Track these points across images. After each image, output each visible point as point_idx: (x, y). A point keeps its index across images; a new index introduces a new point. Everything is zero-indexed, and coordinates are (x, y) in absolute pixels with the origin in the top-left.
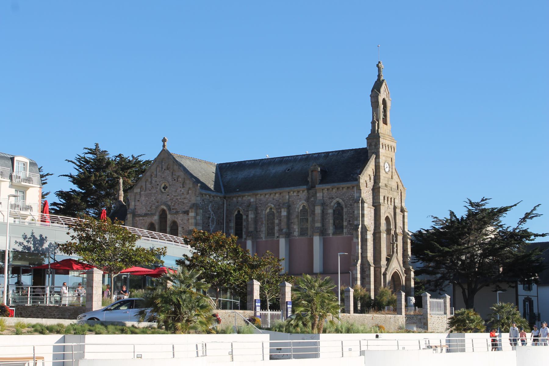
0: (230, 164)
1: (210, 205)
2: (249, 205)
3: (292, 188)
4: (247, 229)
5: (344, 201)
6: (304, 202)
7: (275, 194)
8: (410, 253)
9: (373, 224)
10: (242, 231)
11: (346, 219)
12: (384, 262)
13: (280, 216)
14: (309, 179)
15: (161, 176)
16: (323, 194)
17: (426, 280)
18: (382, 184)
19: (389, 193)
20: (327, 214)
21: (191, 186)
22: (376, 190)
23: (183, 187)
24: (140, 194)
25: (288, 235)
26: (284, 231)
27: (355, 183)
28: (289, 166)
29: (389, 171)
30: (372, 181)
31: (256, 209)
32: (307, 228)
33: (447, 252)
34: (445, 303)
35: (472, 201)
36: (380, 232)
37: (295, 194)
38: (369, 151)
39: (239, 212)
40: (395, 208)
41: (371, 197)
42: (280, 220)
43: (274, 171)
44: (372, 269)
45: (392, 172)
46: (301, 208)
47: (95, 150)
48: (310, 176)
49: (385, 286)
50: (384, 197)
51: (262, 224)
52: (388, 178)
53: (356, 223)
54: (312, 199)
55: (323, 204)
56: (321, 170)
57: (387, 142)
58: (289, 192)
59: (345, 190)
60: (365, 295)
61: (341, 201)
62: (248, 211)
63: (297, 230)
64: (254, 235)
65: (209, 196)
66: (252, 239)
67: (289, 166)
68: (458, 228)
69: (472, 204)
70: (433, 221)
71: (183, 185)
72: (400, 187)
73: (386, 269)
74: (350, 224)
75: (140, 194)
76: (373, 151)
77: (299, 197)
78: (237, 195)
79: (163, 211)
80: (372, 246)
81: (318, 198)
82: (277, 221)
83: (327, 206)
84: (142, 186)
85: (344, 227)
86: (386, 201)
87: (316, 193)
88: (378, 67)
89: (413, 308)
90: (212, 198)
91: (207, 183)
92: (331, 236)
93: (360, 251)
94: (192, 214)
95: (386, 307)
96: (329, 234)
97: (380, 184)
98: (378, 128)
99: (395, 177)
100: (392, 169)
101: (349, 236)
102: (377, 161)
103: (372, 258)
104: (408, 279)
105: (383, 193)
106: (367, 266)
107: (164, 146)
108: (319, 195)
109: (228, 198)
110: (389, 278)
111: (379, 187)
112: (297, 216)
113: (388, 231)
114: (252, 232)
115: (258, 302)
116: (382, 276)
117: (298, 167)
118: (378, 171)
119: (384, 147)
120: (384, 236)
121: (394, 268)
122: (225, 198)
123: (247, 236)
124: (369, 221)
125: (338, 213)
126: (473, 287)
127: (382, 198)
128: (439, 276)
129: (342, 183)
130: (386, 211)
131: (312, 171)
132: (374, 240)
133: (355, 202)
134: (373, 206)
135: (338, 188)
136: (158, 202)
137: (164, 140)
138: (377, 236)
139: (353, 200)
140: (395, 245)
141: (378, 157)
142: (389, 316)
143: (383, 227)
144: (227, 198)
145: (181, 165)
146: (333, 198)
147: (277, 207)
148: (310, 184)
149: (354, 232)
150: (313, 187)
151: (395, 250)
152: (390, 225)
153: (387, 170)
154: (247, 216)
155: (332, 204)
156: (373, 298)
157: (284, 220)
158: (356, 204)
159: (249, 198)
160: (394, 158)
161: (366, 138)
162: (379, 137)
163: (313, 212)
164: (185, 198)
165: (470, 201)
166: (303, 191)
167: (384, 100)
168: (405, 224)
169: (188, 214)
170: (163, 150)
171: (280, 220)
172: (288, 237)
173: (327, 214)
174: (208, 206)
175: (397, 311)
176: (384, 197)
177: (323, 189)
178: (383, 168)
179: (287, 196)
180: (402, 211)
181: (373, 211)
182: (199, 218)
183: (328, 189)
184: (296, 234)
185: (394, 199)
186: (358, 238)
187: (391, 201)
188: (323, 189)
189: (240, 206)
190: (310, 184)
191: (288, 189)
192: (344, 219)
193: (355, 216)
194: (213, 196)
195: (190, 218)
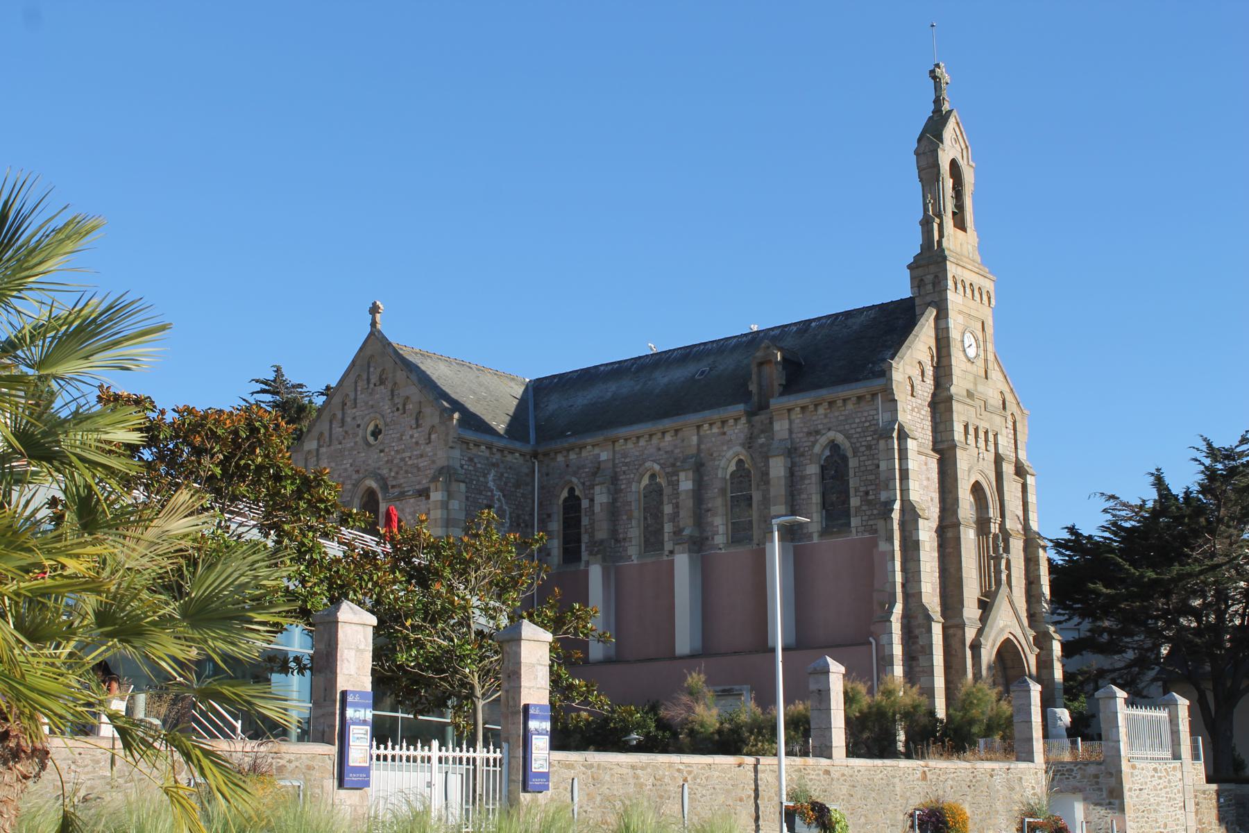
0: (561, 376)
1: (493, 473)
2: (597, 469)
3: (707, 414)
4: (592, 536)
5: (848, 437)
6: (738, 449)
7: (663, 433)
8: (1046, 590)
9: (937, 500)
10: (579, 541)
11: (857, 490)
12: (971, 611)
13: (676, 494)
14: (753, 387)
15: (367, 403)
16: (791, 422)
17: (1095, 667)
18: (958, 386)
19: (979, 416)
20: (803, 478)
21: (436, 420)
22: (941, 405)
23: (418, 426)
24: (318, 455)
25: (698, 544)
26: (687, 532)
27: (877, 383)
28: (704, 366)
29: (978, 355)
30: (930, 381)
31: (615, 480)
32: (751, 522)
33: (1154, 582)
34: (1174, 721)
35: (1216, 445)
36: (957, 525)
37: (715, 430)
38: (917, 301)
39: (572, 490)
40: (998, 460)
41: (928, 424)
42: (677, 506)
43: (666, 380)
44: (937, 630)
45: (986, 360)
46: (732, 467)
47: (274, 381)
48: (754, 377)
49: (977, 676)
50: (966, 427)
51: (630, 519)
52: (976, 377)
53: (883, 496)
54: (762, 440)
55: (792, 452)
56: (783, 358)
57: (969, 277)
58: (699, 427)
59: (850, 406)
60: (915, 707)
61: (840, 438)
62: (592, 487)
63: (721, 529)
64: (610, 553)
65: (489, 447)
66: (604, 560)
67: (704, 366)
68: (1178, 519)
69: (1212, 452)
70: (1105, 511)
71: (417, 420)
72: (1012, 406)
73: (980, 632)
74: (869, 503)
75: (318, 455)
76: (928, 299)
77: (727, 438)
78: (566, 445)
79: (371, 493)
80: (936, 564)
81: (778, 436)
82: (668, 509)
83: (802, 455)
84: (321, 434)
85: (852, 511)
86: (971, 438)
87: (771, 423)
88: (934, 77)
89: (1067, 742)
90: (498, 456)
91: (487, 418)
92: (816, 539)
93: (899, 578)
94: (436, 496)
95: (982, 741)
96: (810, 536)
97: (953, 390)
98: (941, 235)
99: (995, 374)
100: (985, 351)
101: (867, 535)
102: (942, 325)
103: (937, 600)
104: (1045, 663)
105: (961, 414)
106: (920, 619)
107: (374, 324)
108: (780, 427)
109: (546, 454)
110: (988, 654)
111: (950, 398)
112: (723, 491)
113: (982, 525)
114: (602, 542)
115: (356, 706)
116: (969, 653)
117: (727, 364)
118: (944, 352)
119: (959, 286)
120: (969, 536)
121: (1002, 630)
122: (535, 455)
123: (591, 553)
124: (922, 487)
125: (835, 470)
126: (1229, 685)
127: (958, 429)
128: (1130, 655)
129: (840, 388)
130: (972, 466)
131: (761, 364)
132: (942, 547)
133: (881, 437)
134: (934, 450)
135: (831, 404)
136: (357, 472)
137: (374, 310)
138: (950, 534)
139: (875, 432)
140: (1003, 562)
141: (942, 315)
142: (988, 765)
143: (966, 507)
144: (540, 457)
145: (426, 382)
146: (817, 432)
147: (669, 470)
148: (755, 398)
149: (881, 523)
150: (763, 406)
151: (1004, 577)
152: (987, 508)
153: (971, 352)
154: (592, 500)
155: (817, 449)
156: (941, 713)
157: (687, 503)
158: (882, 443)
159: (597, 451)
160: (989, 323)
161: (909, 267)
162: (945, 258)
163: (765, 474)
164: (422, 456)
165: (1209, 445)
166: (736, 420)
167: (954, 164)
168: (1031, 507)
169: (428, 497)
170: (371, 334)
171: (677, 506)
172: (699, 551)
173: (803, 478)
174: (485, 476)
175: (1017, 749)
176: (966, 427)
177: (789, 410)
178: (959, 345)
179: (695, 439)
180: (1020, 471)
181: (934, 465)
182: (454, 505)
183: (803, 409)
184: (720, 539)
185: (996, 435)
186: (890, 539)
187: (986, 441)
188: (789, 410)
189: (575, 474)
190: (755, 398)
191: (694, 418)
192: (851, 489)
193: (883, 477)
194: (501, 451)
195: (431, 506)
